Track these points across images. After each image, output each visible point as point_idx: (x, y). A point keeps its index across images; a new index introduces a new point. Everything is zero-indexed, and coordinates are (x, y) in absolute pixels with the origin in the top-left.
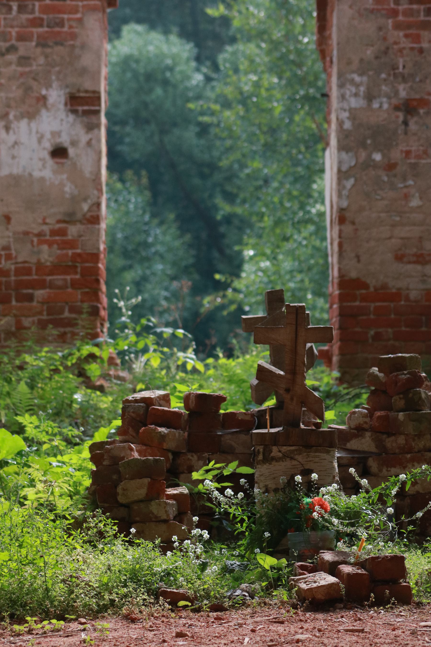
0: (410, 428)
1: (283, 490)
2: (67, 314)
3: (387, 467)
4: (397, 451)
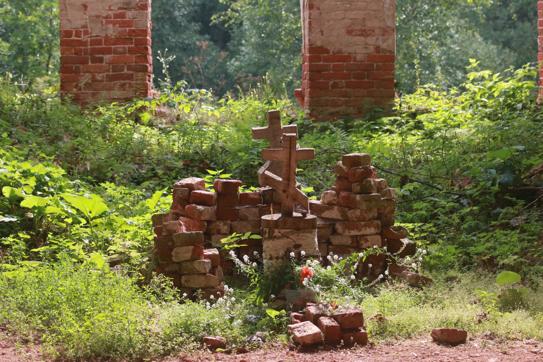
0: (364, 206)
1: (282, 258)
2: (125, 71)
4: (355, 219)
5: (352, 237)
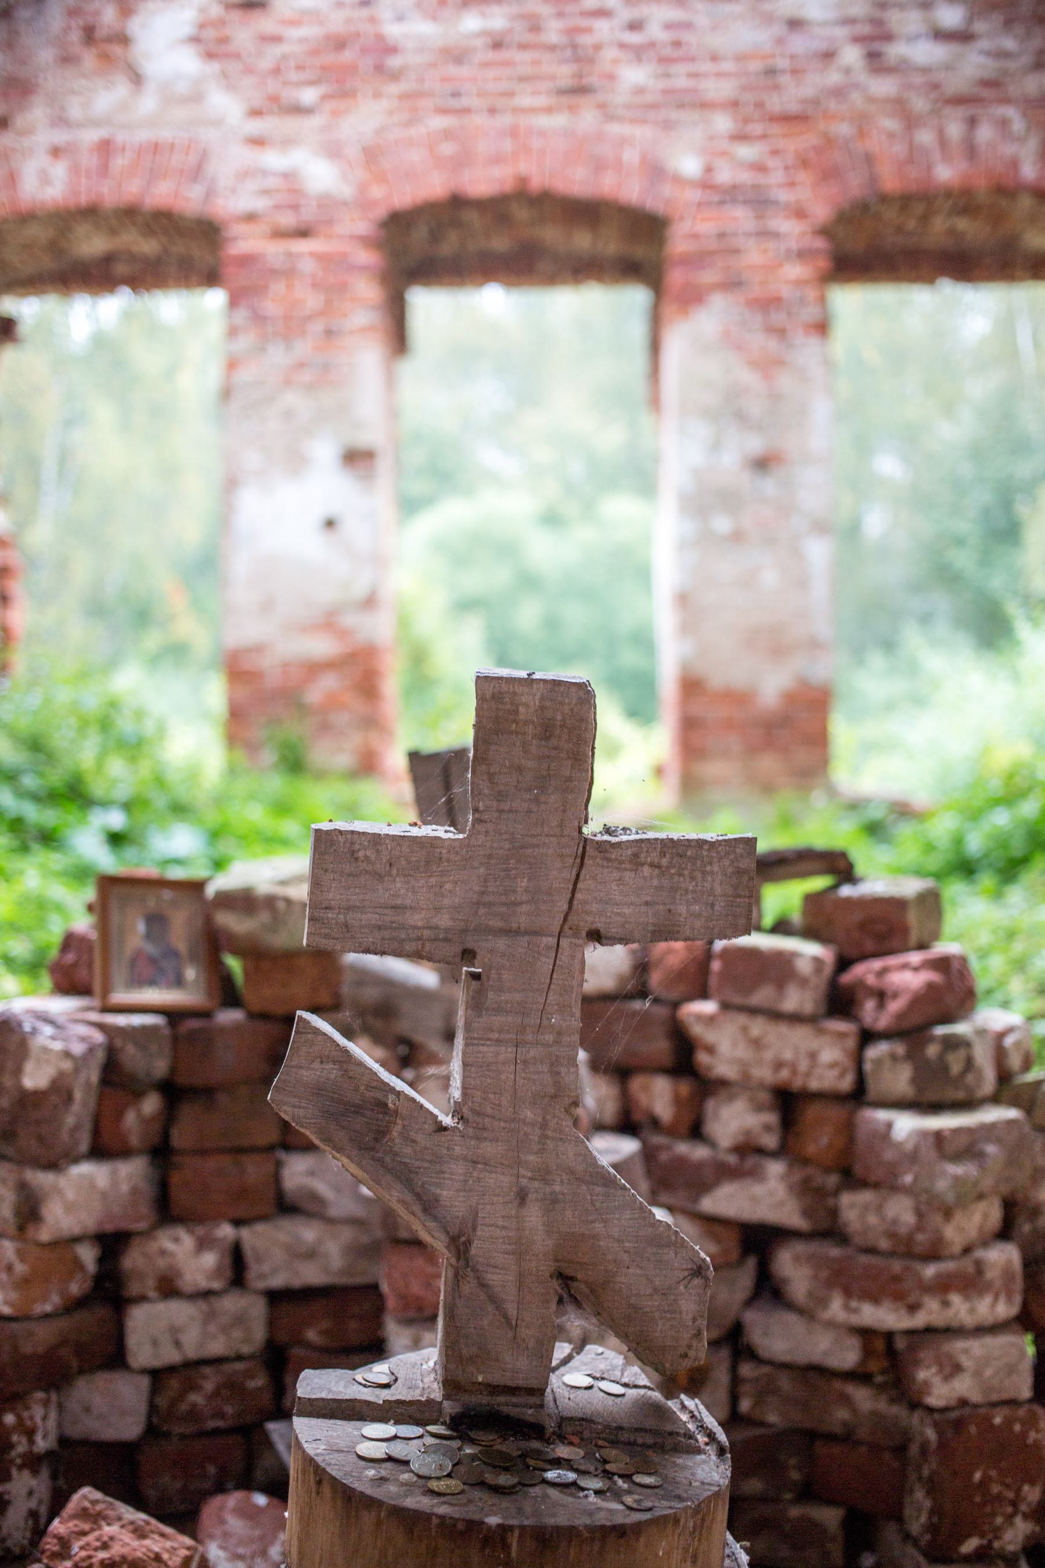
3: (848, 1293)
4: (884, 1244)
5: (866, 1334)
